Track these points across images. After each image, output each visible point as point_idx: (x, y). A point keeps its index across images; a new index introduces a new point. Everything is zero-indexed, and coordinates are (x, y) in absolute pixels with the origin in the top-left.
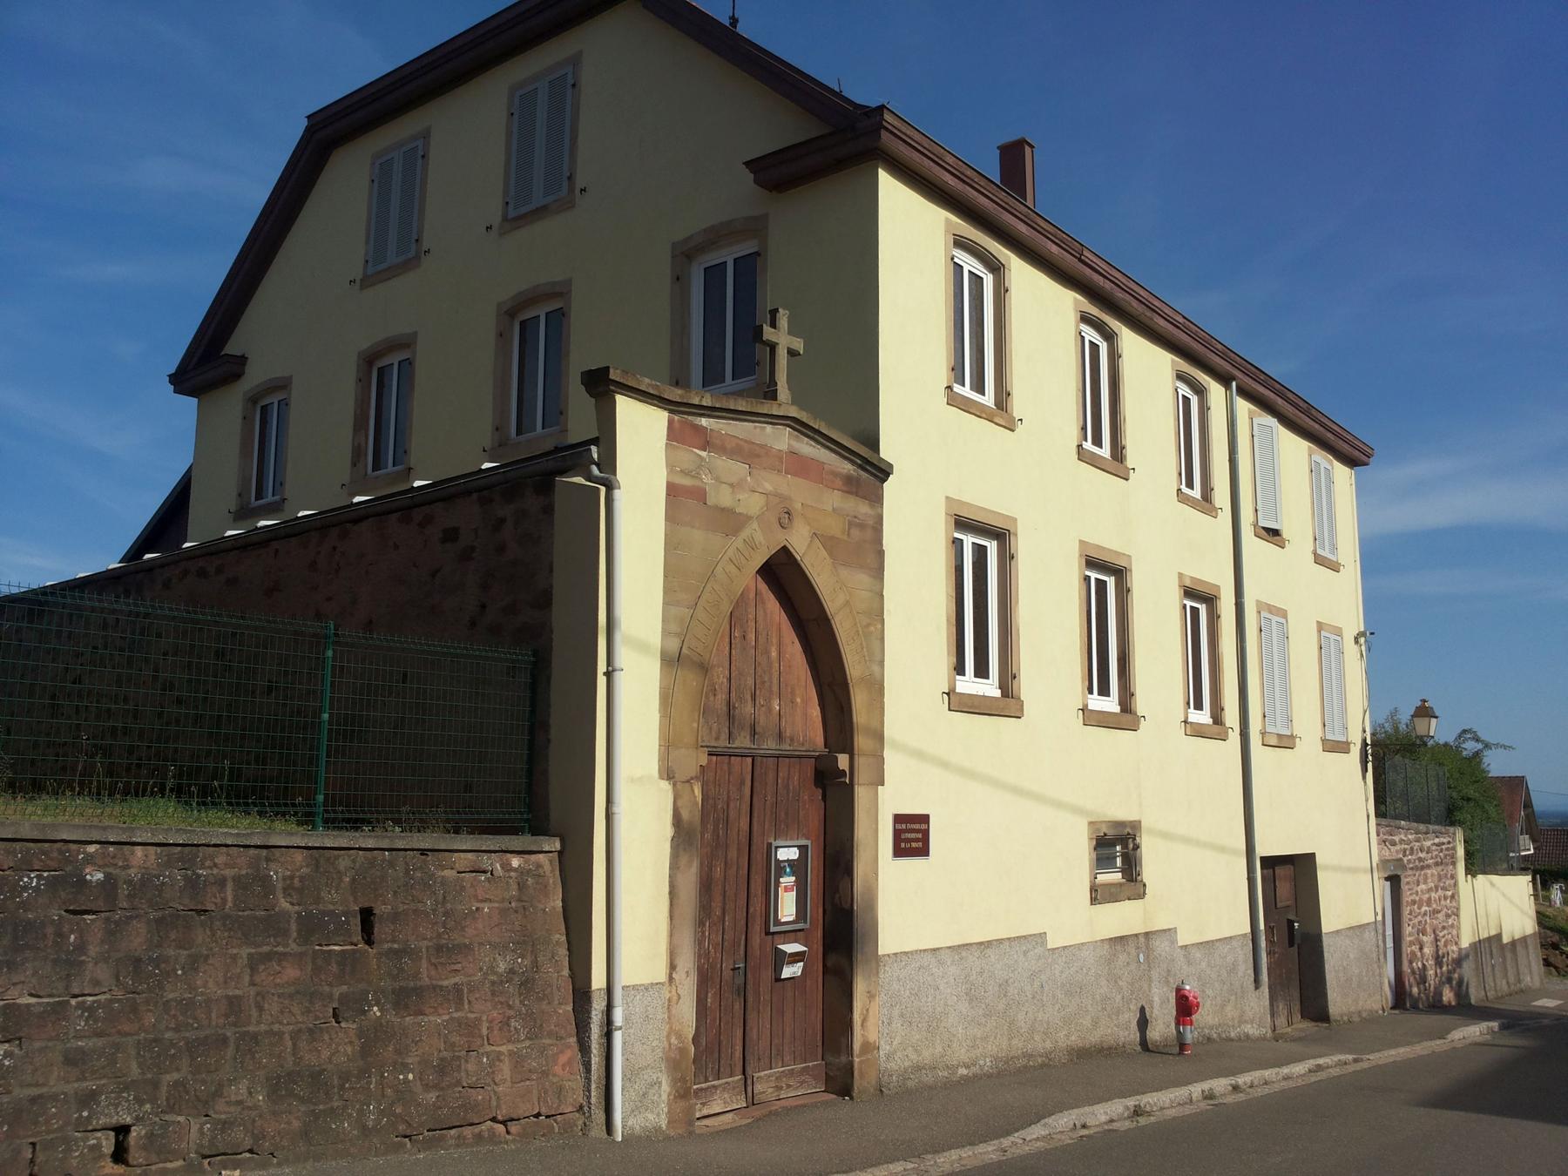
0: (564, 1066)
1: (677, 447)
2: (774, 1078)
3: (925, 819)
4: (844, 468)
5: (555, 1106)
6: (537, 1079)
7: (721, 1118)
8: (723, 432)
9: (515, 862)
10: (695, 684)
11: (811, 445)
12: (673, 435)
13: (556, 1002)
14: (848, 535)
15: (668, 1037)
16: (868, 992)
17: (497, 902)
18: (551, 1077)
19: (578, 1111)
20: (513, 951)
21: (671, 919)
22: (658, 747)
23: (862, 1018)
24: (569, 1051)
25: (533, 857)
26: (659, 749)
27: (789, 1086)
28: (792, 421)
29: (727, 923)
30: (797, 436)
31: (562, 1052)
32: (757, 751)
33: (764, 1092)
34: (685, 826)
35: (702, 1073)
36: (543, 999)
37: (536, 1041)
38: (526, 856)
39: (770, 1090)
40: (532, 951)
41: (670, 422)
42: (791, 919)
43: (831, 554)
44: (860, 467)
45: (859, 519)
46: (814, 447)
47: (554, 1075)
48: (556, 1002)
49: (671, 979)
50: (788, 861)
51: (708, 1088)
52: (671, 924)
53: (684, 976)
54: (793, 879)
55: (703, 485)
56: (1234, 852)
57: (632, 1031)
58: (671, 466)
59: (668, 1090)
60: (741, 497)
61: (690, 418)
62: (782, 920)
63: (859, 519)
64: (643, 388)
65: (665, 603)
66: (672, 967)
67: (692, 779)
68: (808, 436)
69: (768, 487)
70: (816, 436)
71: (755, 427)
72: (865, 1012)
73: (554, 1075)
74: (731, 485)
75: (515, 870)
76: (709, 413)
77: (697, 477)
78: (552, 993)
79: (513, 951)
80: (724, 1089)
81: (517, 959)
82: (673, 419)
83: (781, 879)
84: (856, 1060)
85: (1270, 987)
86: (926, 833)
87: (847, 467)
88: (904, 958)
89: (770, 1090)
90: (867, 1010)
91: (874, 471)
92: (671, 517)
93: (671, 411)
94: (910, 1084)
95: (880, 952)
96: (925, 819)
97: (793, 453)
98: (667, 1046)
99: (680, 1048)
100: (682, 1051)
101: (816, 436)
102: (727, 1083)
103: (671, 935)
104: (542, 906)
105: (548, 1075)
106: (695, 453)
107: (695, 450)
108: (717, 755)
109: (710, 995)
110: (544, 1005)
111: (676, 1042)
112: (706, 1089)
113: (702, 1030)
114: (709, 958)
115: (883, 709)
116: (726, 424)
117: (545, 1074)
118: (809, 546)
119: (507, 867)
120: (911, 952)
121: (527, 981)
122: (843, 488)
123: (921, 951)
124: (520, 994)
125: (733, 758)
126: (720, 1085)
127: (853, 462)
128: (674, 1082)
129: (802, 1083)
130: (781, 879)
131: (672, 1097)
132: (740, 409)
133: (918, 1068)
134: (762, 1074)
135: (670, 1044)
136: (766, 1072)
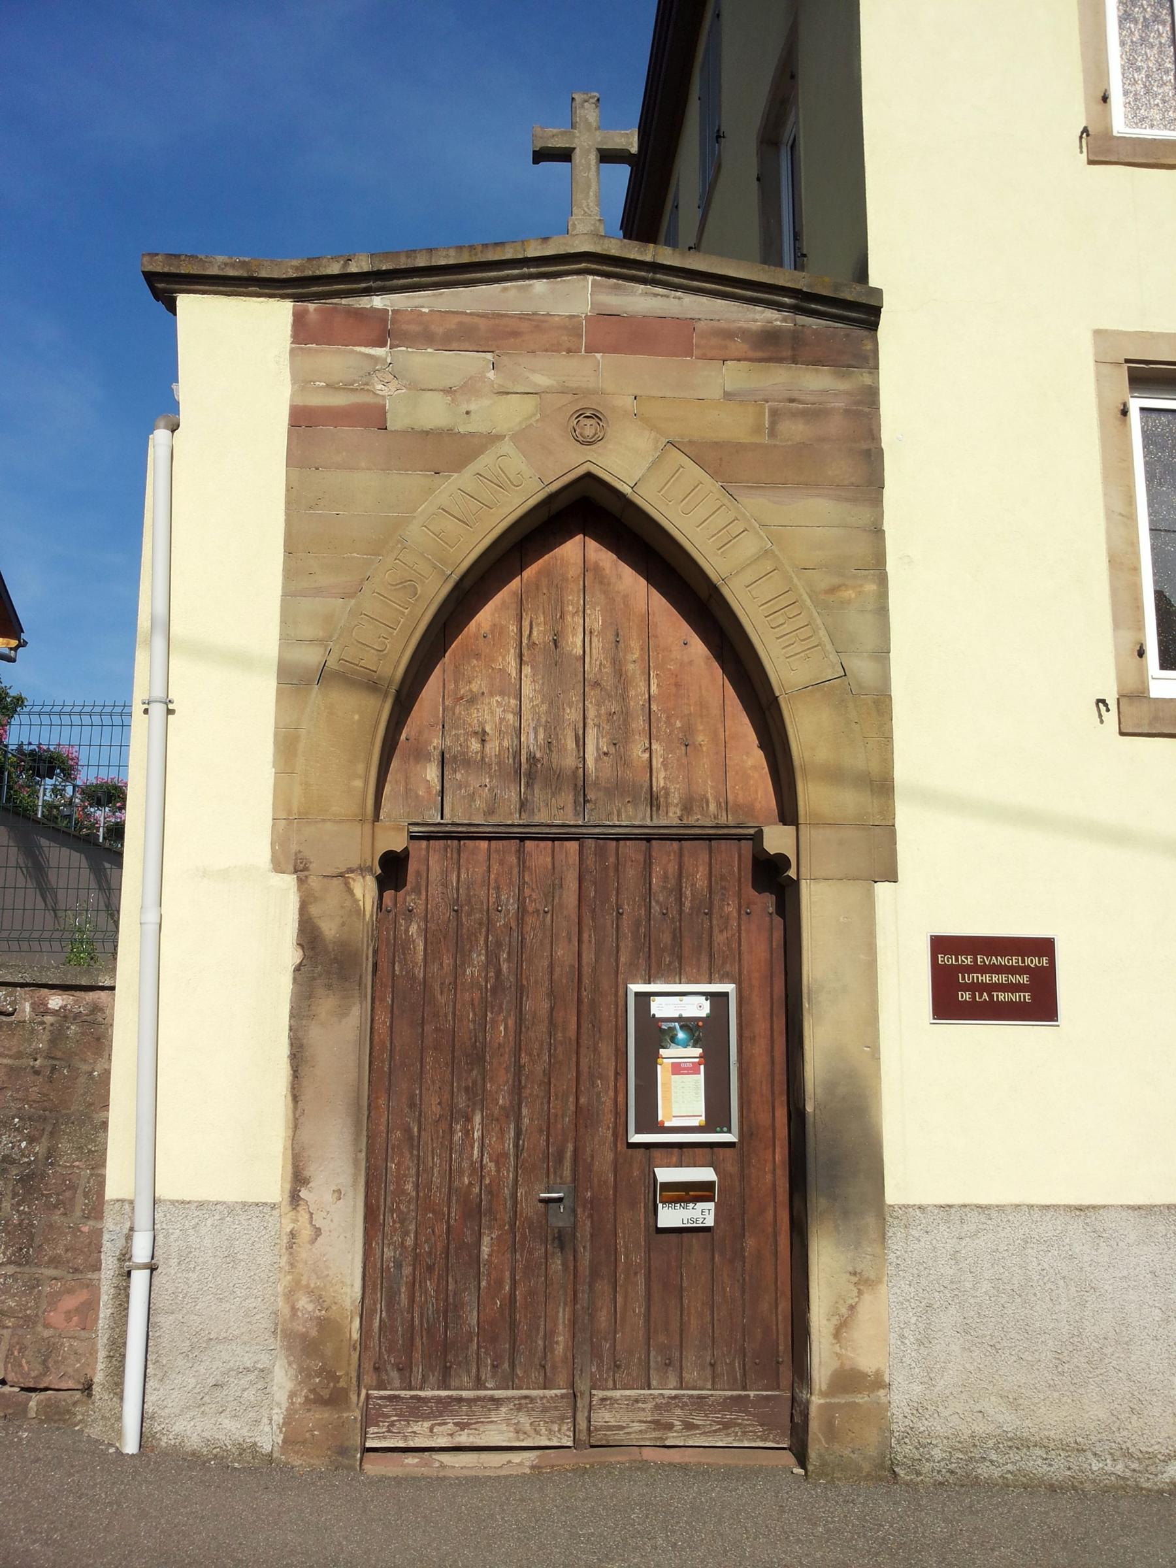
0: (69, 1315)
1: (316, 350)
2: (649, 1406)
3: (1045, 947)
4: (756, 321)
5: (33, 1374)
6: (14, 1328)
7: (486, 1457)
8: (426, 310)
9: (56, 1001)
10: (357, 717)
11: (656, 295)
12: (302, 332)
13: (78, 1213)
14: (772, 433)
15: (290, 1295)
16: (854, 1274)
17: (10, 1057)
18: (39, 1328)
19: (82, 1391)
20: (17, 1130)
21: (295, 1098)
22: (270, 822)
23: (835, 1321)
24: (85, 1291)
25: (91, 996)
26: (273, 826)
27: (689, 1426)
28: (588, 262)
29: (526, 1121)
30: (616, 287)
31: (70, 1291)
32: (584, 831)
33: (621, 1428)
34: (330, 948)
35: (468, 1372)
36: (55, 1207)
37: (27, 1269)
38: (78, 994)
39: (637, 1426)
40: (51, 1133)
41: (299, 320)
42: (697, 1124)
43: (715, 474)
44: (796, 309)
45: (800, 402)
46: (667, 296)
47: (47, 1326)
48: (78, 1213)
49: (295, 1199)
50: (680, 1019)
51: (478, 1399)
52: (295, 1109)
53: (329, 1197)
54: (698, 1051)
55: (379, 401)
56: (928, 798)
57: (194, 1276)
58: (301, 381)
59: (289, 1385)
60: (472, 407)
61: (344, 301)
62: (667, 1124)
63: (800, 402)
64: (214, 271)
65: (289, 594)
66: (299, 1179)
67: (351, 870)
68: (644, 281)
69: (541, 380)
70: (658, 276)
71: (505, 289)
72: (844, 1310)
73: (47, 1326)
74: (449, 391)
75: (55, 1013)
76: (379, 283)
77: (366, 387)
78: (73, 1199)
79: (17, 1130)
80: (519, 1408)
81: (20, 1141)
82: (306, 311)
83: (662, 1051)
84: (816, 1401)
85: (732, 1395)
86: (1051, 972)
87: (762, 317)
88: (974, 1216)
89: (637, 1426)
90: (852, 1308)
91: (834, 311)
92: (297, 459)
93: (297, 298)
94: (983, 1470)
95: (892, 1196)
96: (1045, 947)
97: (605, 316)
98: (286, 1311)
99: (319, 1318)
100: (327, 1326)
101: (658, 276)
102: (526, 1397)
103: (296, 1125)
104: (85, 1068)
105: (35, 1323)
106: (360, 353)
107: (357, 349)
108: (489, 839)
109: (486, 1240)
110: (57, 1218)
111: (310, 1307)
112: (470, 1401)
113: (369, 1291)
114: (482, 1177)
115: (889, 739)
116: (434, 295)
117: (29, 1322)
118: (655, 464)
119: (41, 1009)
120: (1000, 1208)
121: (31, 1176)
122: (759, 354)
123: (1031, 1207)
124: (15, 1195)
125: (528, 843)
126: (509, 1399)
127: (778, 306)
128: (304, 1374)
129: (726, 1426)
130: (662, 1051)
131: (300, 1400)
132: (443, 262)
133: (1020, 1443)
134: (618, 1394)
135: (294, 1310)
136: (628, 1392)
